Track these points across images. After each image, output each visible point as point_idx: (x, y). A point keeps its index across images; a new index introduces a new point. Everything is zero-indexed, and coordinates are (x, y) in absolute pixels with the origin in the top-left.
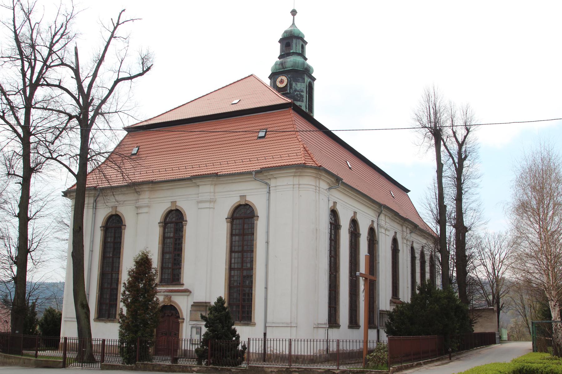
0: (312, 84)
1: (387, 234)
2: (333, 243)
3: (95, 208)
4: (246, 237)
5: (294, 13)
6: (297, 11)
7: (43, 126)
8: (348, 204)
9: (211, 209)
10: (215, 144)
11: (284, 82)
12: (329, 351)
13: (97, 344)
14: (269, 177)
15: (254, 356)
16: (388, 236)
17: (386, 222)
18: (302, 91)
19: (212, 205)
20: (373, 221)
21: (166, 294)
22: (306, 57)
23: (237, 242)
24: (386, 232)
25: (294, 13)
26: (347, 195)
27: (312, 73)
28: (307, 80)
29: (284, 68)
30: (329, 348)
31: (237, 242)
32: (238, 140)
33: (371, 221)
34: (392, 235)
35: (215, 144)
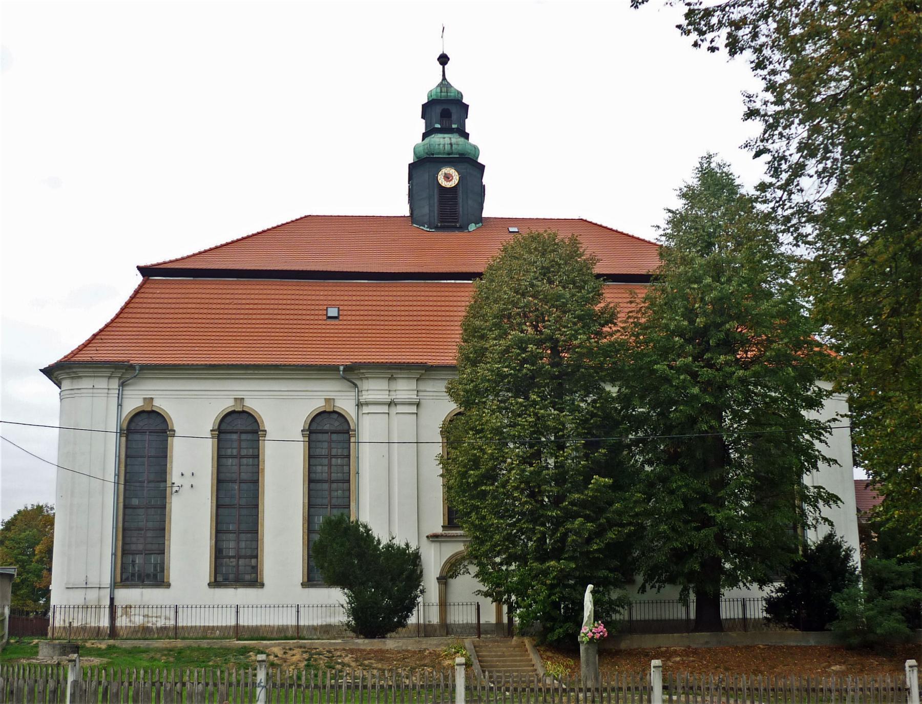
5: (443, 60)
10: (168, 311)
11: (451, 180)
25: (443, 60)
35: (168, 311)
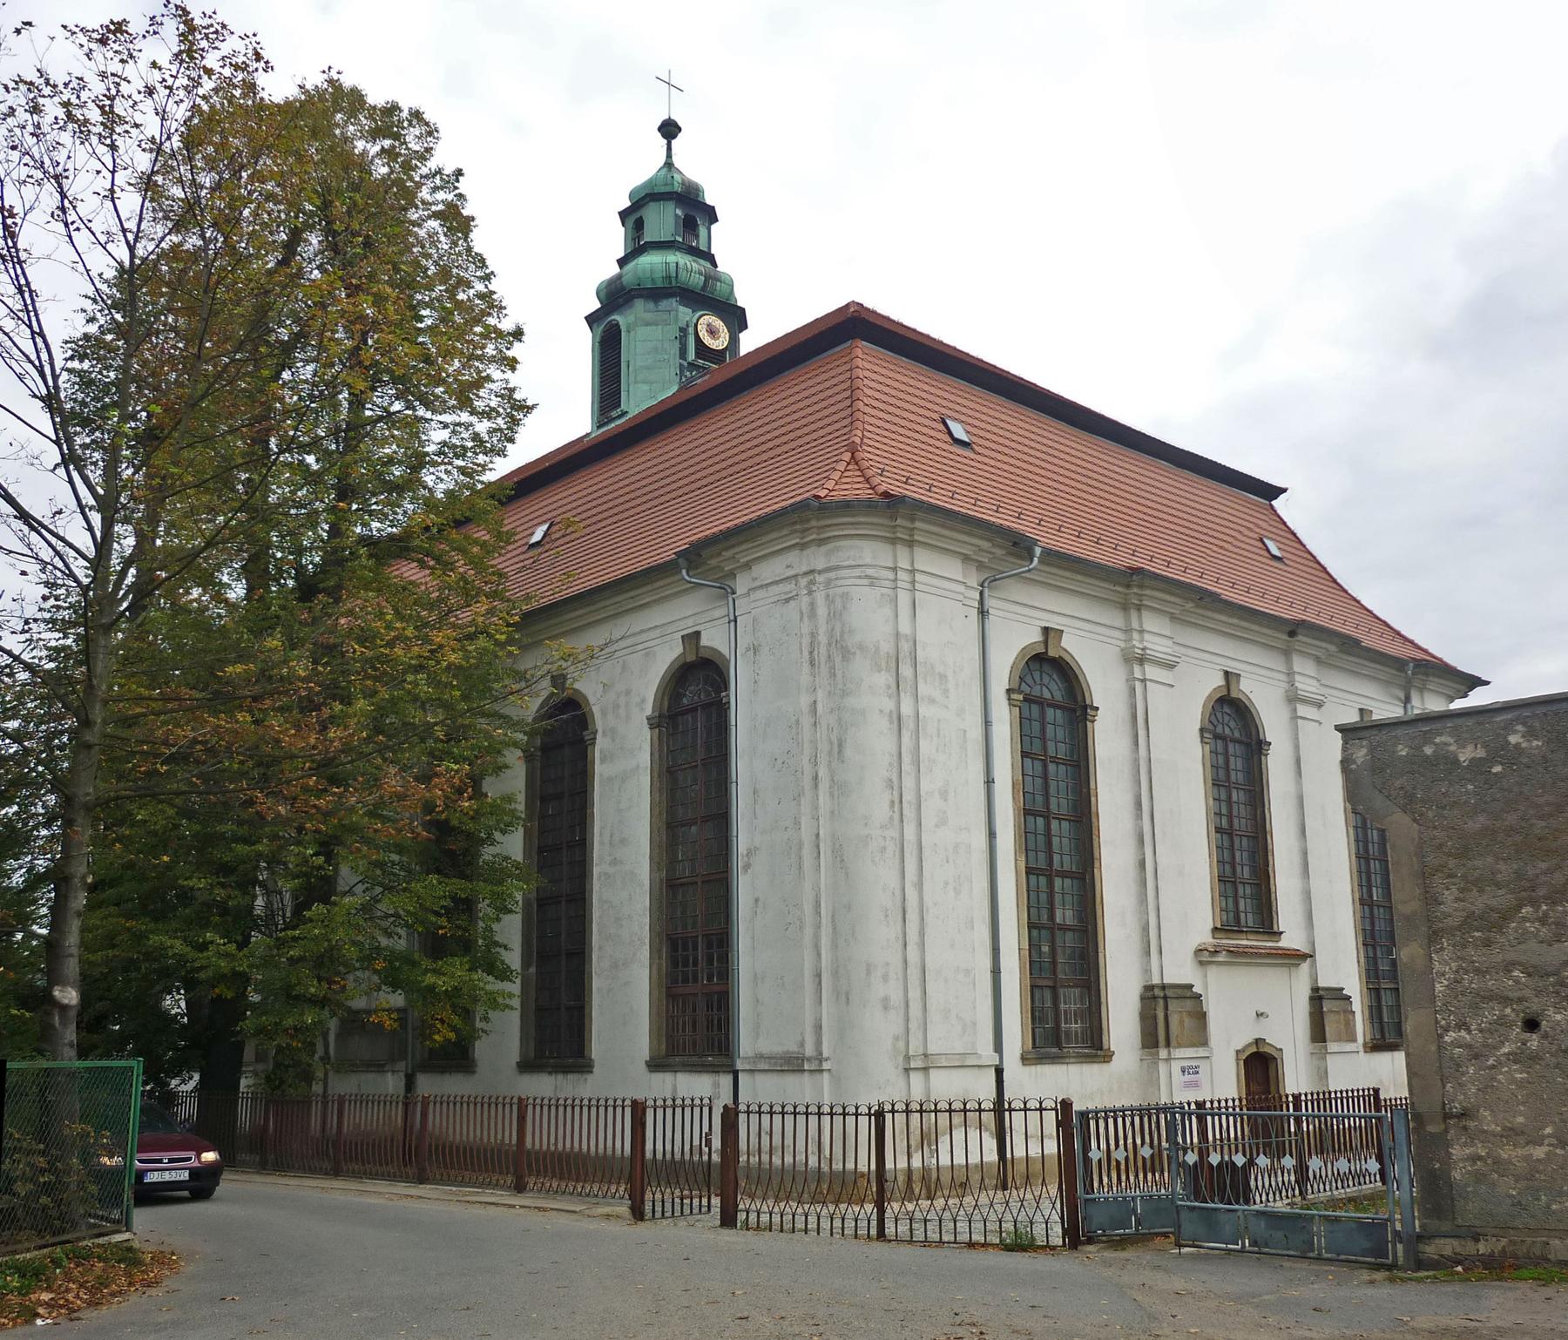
5: (669, 130)
7: (33, 357)
25: (669, 130)
26: (1050, 585)
32: (811, 419)
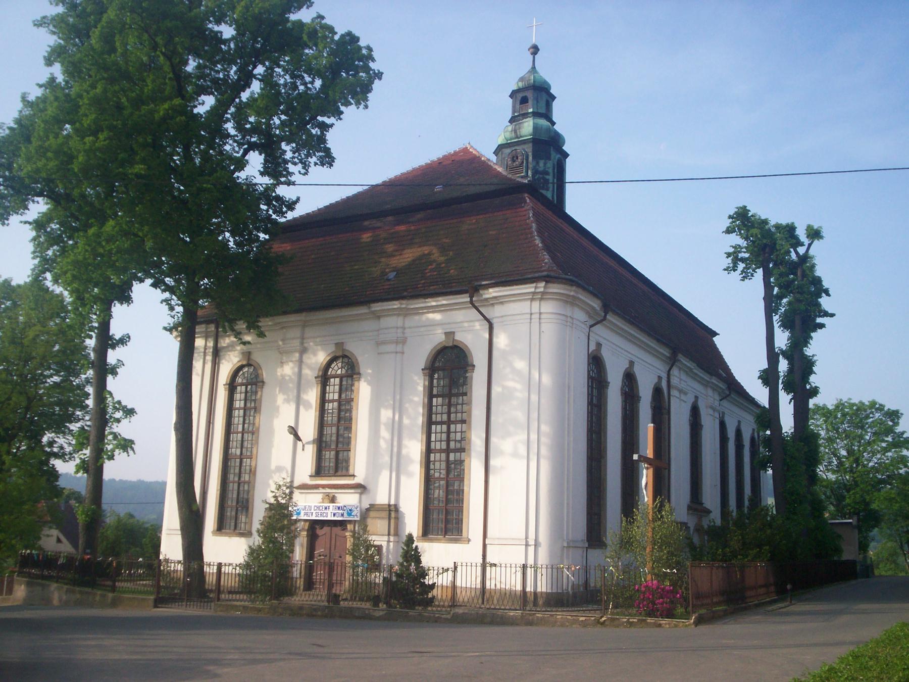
0: (562, 163)
1: (682, 398)
2: (595, 411)
3: (217, 354)
4: (454, 400)
5: (535, 50)
6: (539, 47)
8: (620, 347)
9: (398, 354)
12: (588, 586)
13: (228, 573)
14: (491, 302)
15: (464, 593)
16: (685, 402)
17: (681, 379)
18: (548, 174)
19: (399, 348)
20: (660, 378)
21: (328, 490)
22: (554, 119)
23: (439, 408)
24: (680, 396)
25: (535, 50)
27: (550, 89)
28: (555, 156)
29: (517, 137)
30: (588, 581)
31: (439, 408)
33: (657, 377)
34: (690, 399)
